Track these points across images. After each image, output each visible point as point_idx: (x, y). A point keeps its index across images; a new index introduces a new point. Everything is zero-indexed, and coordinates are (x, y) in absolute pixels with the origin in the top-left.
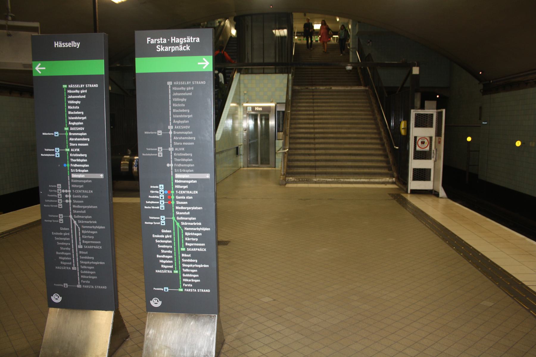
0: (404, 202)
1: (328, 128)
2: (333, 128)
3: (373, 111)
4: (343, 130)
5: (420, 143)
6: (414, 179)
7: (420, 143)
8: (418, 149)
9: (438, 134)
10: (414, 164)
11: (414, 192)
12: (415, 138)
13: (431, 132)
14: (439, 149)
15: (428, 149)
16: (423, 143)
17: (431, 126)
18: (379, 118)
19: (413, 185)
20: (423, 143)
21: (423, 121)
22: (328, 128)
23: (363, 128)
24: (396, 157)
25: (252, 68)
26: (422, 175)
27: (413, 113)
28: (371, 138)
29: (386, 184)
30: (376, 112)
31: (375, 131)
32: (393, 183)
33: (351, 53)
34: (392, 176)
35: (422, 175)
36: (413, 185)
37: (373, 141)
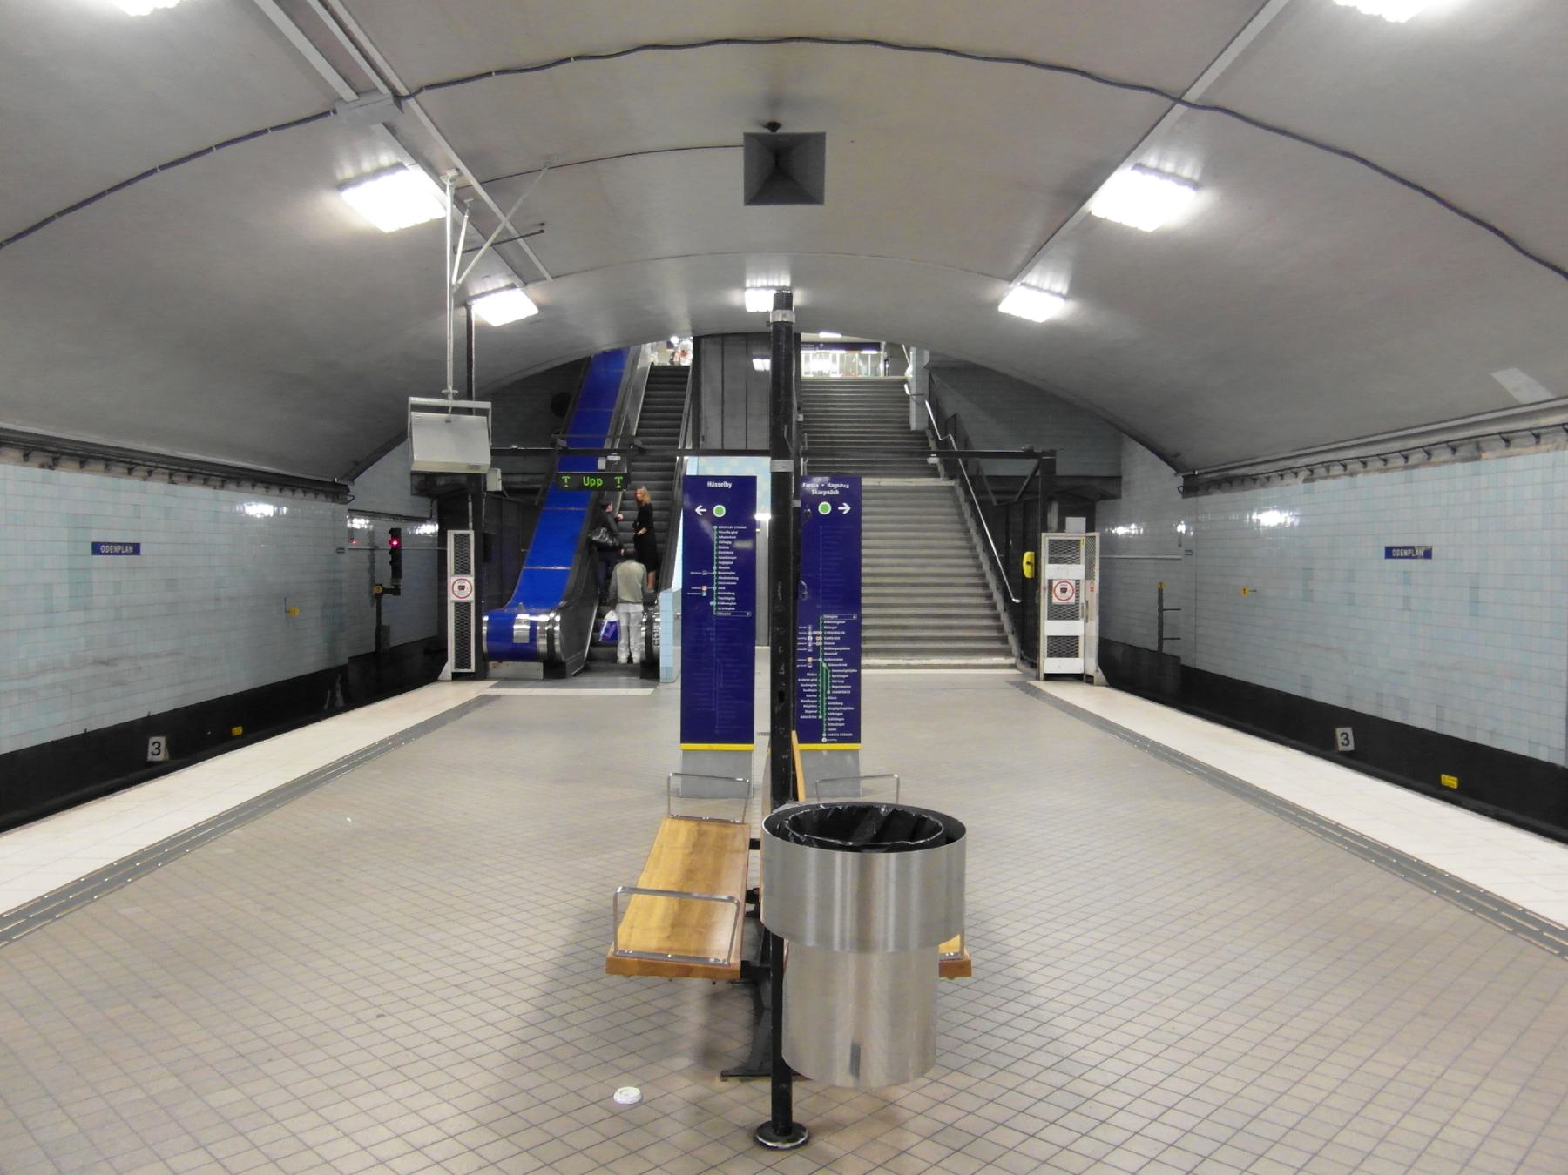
0: (1035, 692)
1: (882, 566)
2: (892, 566)
3: (961, 514)
4: (911, 570)
5: (1058, 591)
6: (1051, 655)
7: (1058, 591)
8: (1055, 601)
9: (1089, 575)
10: (1051, 628)
11: (1050, 677)
12: (1050, 581)
13: (1076, 571)
14: (1091, 596)
15: (1072, 601)
16: (1064, 590)
17: (1078, 562)
18: (979, 549)
19: (1050, 665)
20: (1064, 590)
21: (1064, 552)
22: (882, 566)
23: (949, 566)
24: (1020, 623)
25: (592, 644)
26: (1065, 646)
27: (1046, 539)
28: (968, 585)
29: (999, 669)
30: (973, 532)
31: (994, 634)
32: (1013, 666)
33: (913, 405)
34: (1008, 654)
35: (1065, 646)
36: (1050, 665)
37: (985, 634)
